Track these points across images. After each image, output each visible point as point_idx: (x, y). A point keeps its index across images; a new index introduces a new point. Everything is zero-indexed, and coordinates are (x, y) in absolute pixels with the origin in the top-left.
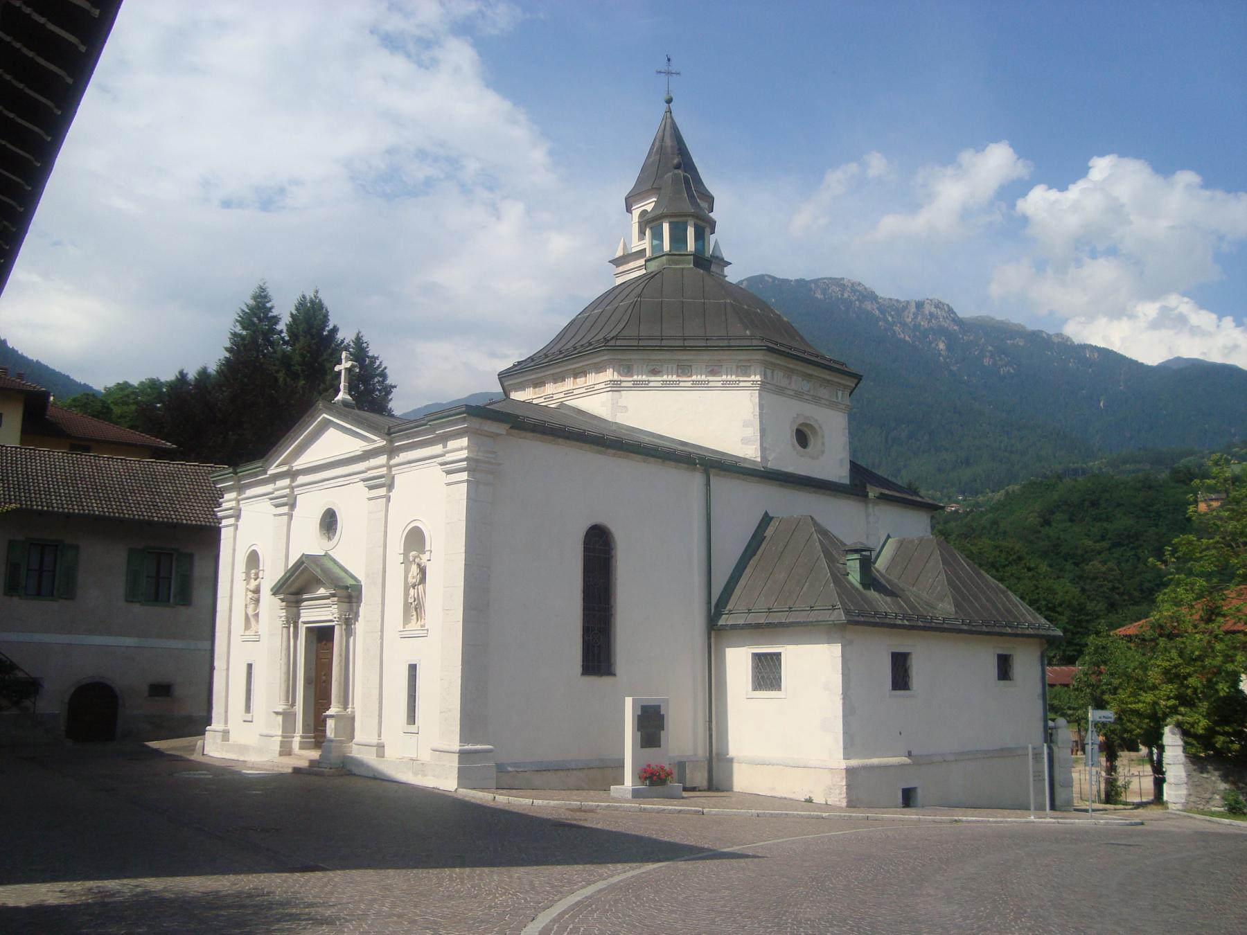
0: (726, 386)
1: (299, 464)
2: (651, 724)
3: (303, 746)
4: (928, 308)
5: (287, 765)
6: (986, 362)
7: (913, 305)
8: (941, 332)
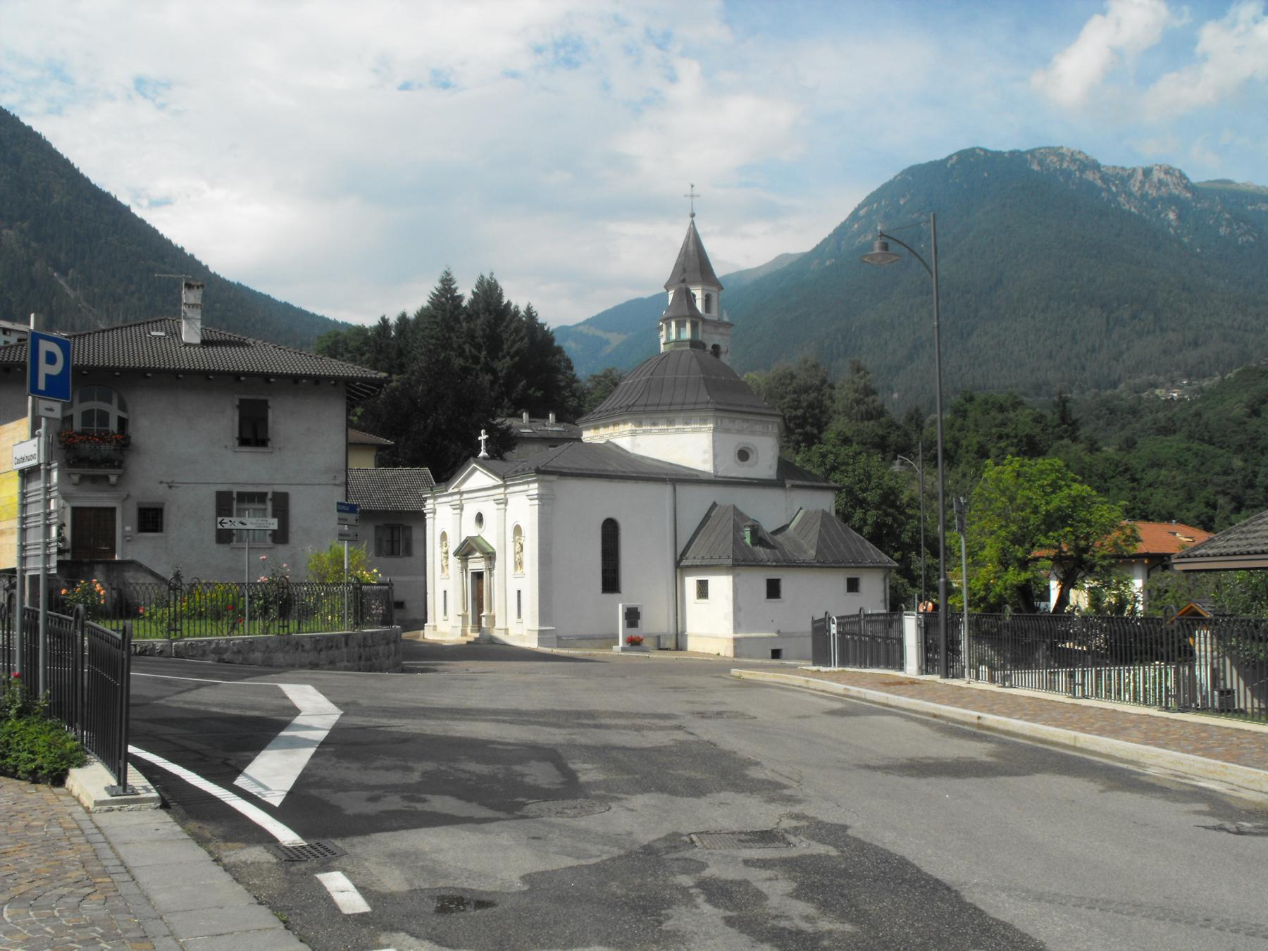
0: (694, 431)
1: (464, 487)
2: (632, 616)
3: (472, 631)
4: (1157, 175)
5: (464, 640)
6: (1222, 231)
7: (1140, 172)
8: (1172, 200)
